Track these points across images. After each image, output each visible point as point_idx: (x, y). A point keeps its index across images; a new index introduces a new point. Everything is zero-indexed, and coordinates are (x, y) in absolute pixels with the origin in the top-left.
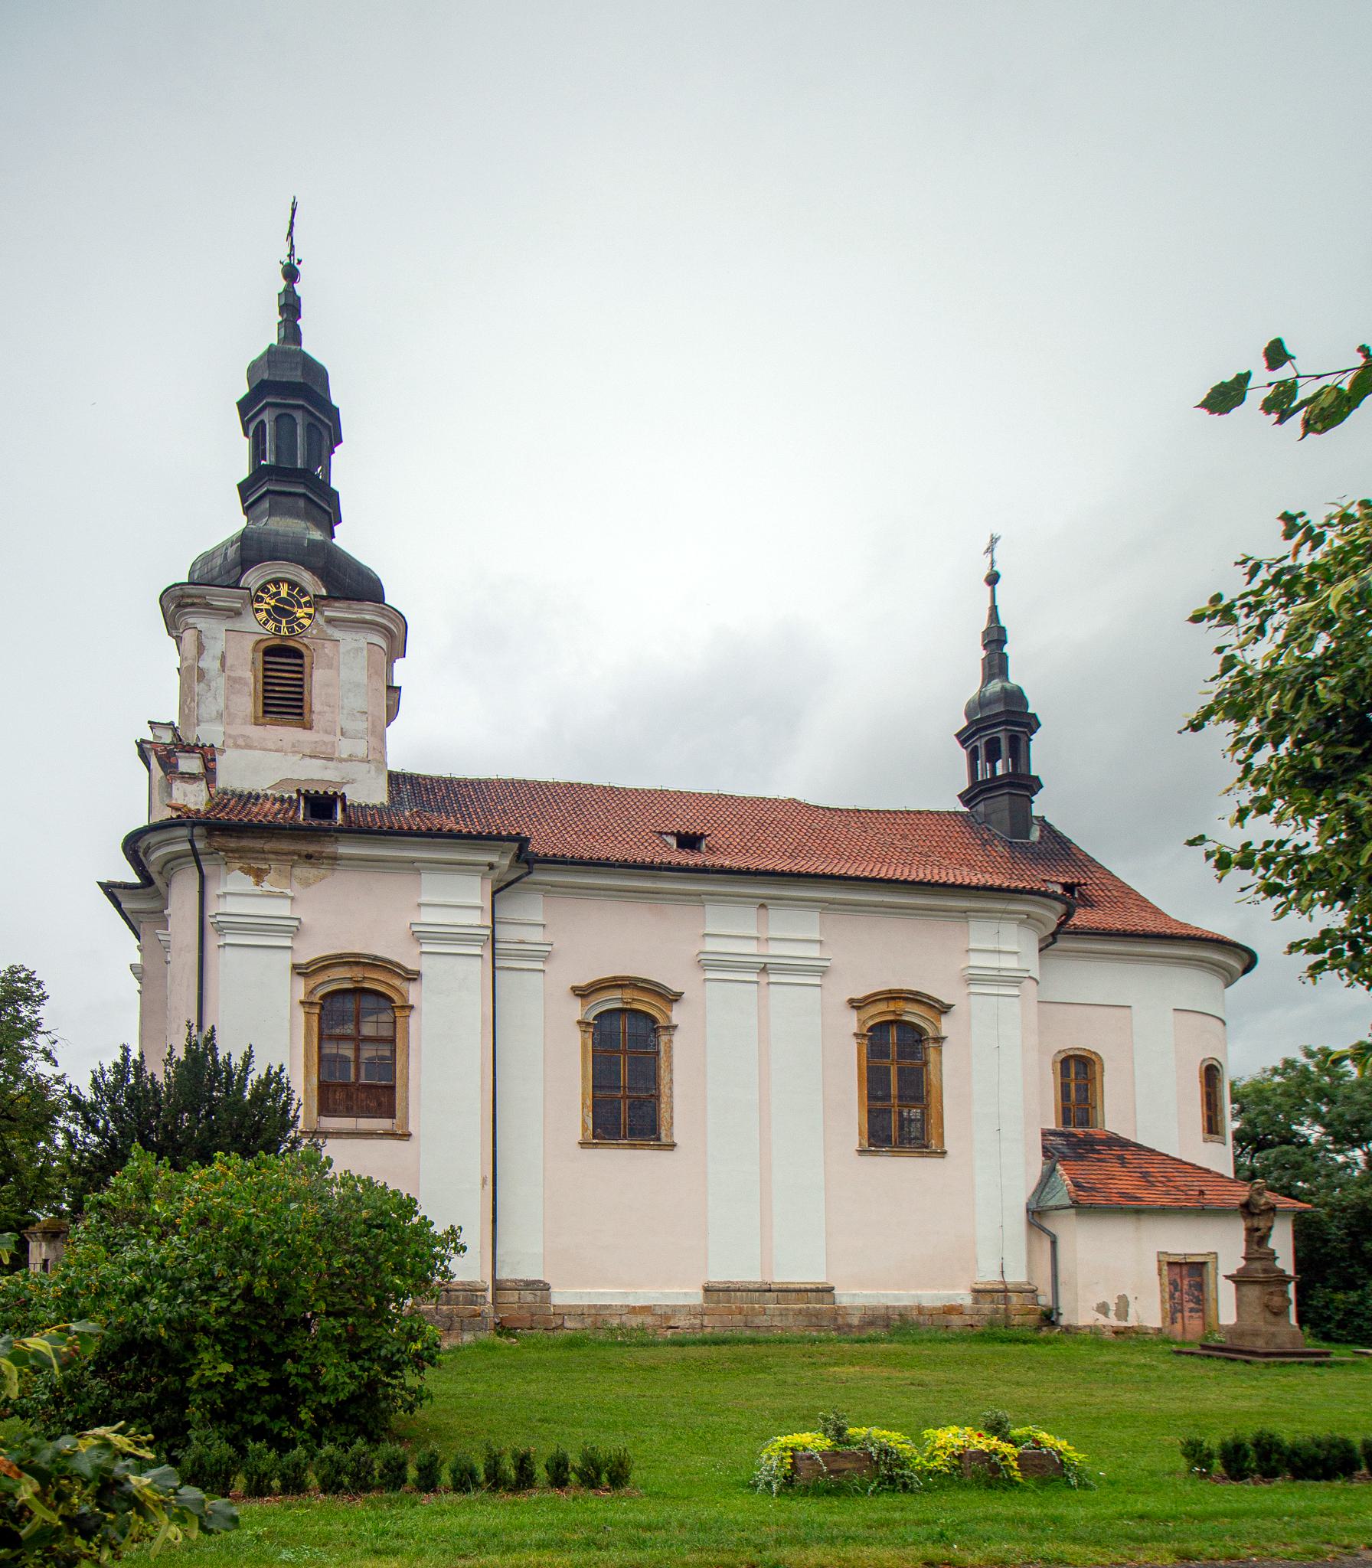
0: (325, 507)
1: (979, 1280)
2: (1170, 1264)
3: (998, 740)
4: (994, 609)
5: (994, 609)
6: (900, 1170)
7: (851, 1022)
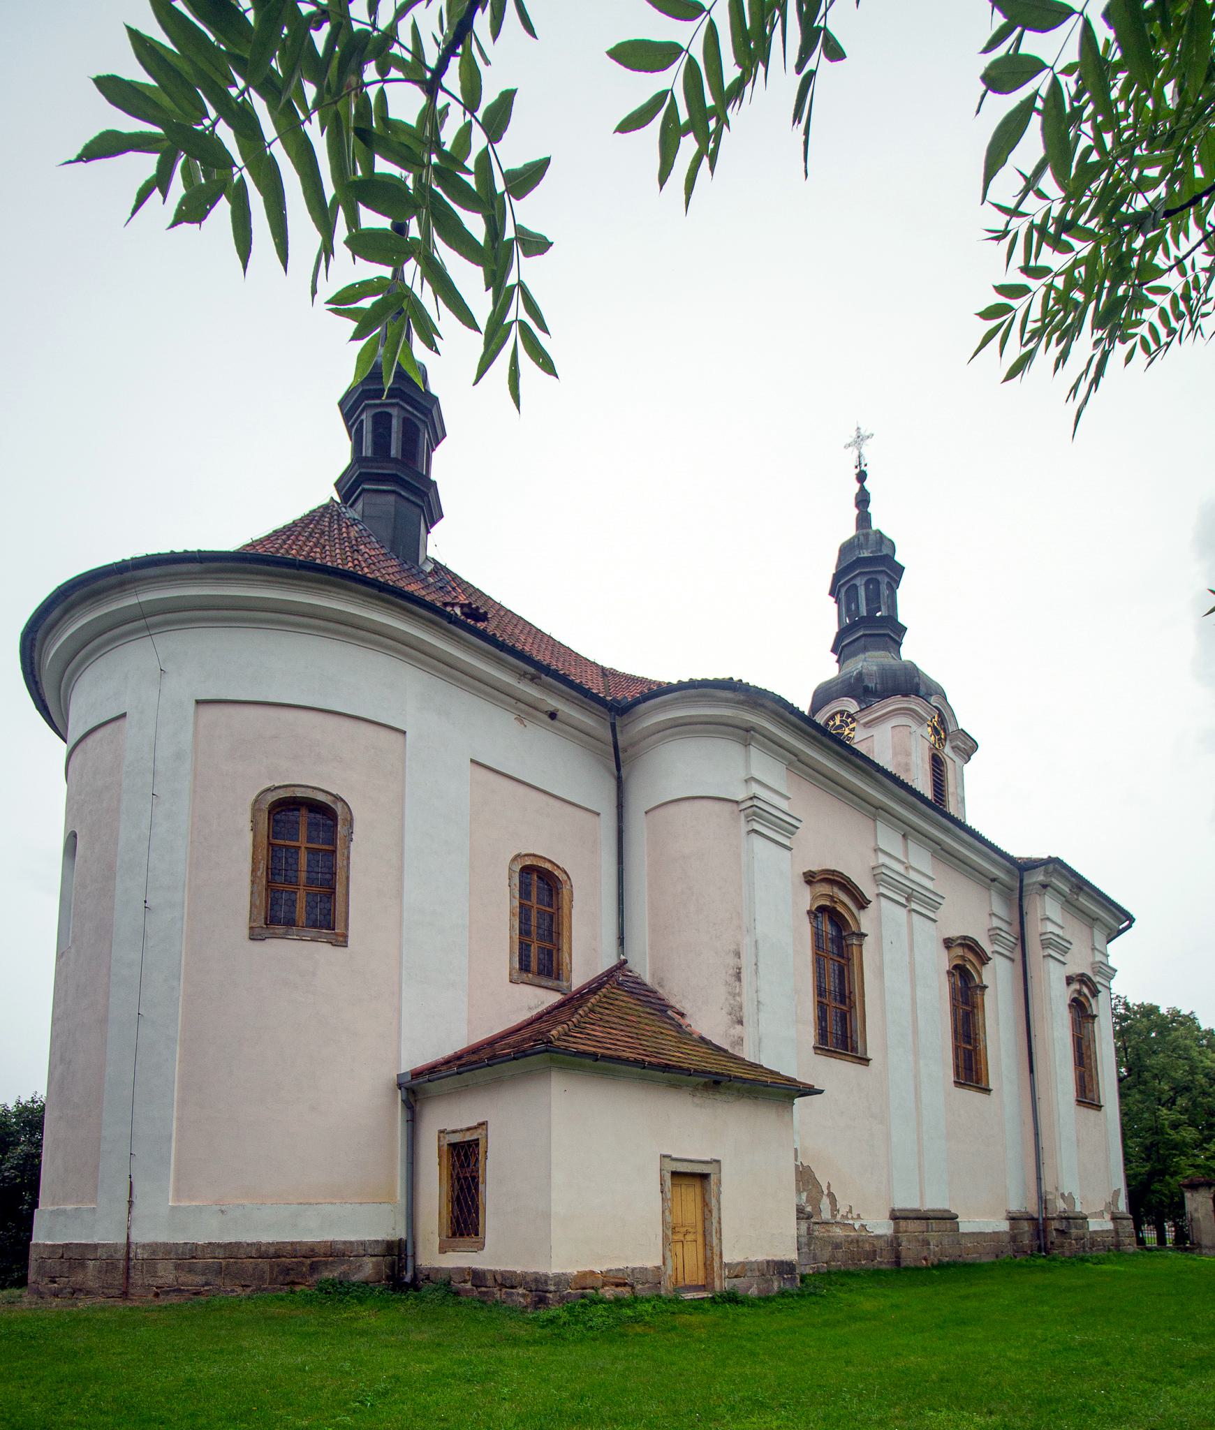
0: (892, 632)
3: (855, 587)
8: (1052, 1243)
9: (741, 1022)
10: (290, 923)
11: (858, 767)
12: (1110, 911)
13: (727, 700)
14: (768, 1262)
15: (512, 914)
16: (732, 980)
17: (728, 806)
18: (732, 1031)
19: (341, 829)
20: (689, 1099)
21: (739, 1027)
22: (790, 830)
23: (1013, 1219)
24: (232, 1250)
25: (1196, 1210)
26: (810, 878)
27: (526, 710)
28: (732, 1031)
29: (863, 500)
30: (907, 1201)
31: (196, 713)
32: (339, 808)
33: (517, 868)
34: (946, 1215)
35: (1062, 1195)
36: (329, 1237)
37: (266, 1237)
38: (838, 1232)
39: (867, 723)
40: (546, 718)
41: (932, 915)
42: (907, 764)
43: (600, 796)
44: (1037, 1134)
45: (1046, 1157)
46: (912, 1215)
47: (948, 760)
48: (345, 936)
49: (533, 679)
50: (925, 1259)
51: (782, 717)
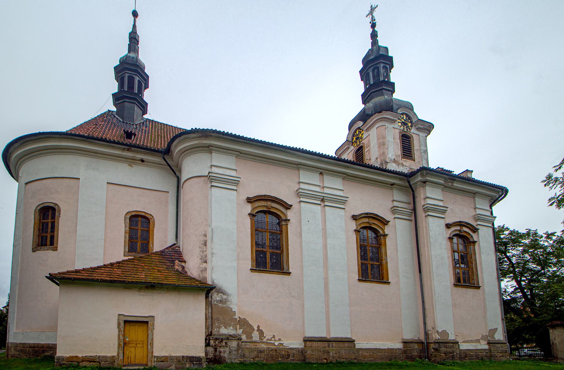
1: (307, 336)
2: (126, 322)
4: (134, 26)
5: (134, 26)
6: (269, 280)
7: (353, 225)
8: (431, 355)
9: (206, 262)
10: (46, 245)
11: (276, 150)
12: (483, 187)
13: (194, 138)
14: (183, 357)
15: (126, 232)
16: (202, 246)
17: (202, 179)
18: (201, 266)
19: (57, 214)
20: (137, 293)
21: (205, 264)
22: (237, 183)
23: (405, 343)
24: (24, 344)
25: (555, 339)
26: (250, 200)
27: (131, 161)
28: (201, 266)
29: (374, 35)
30: (311, 333)
31: (25, 187)
32: (56, 207)
33: (128, 216)
34: (351, 340)
35: (437, 331)
36: (48, 342)
37: (32, 342)
38: (264, 346)
39: (367, 129)
40: (140, 162)
41: (343, 207)
42: (383, 142)
43: (169, 185)
44: (423, 302)
45: (427, 313)
46: (345, 340)
47: (414, 135)
48: (57, 247)
49: (128, 150)
50: (326, 359)
51: (219, 137)
